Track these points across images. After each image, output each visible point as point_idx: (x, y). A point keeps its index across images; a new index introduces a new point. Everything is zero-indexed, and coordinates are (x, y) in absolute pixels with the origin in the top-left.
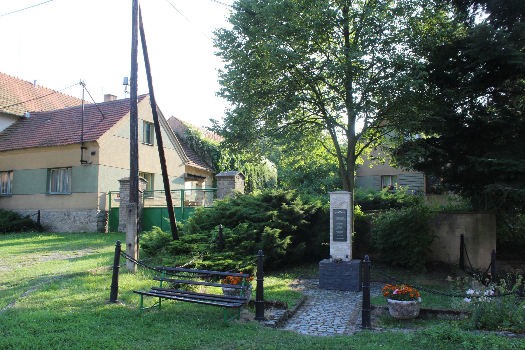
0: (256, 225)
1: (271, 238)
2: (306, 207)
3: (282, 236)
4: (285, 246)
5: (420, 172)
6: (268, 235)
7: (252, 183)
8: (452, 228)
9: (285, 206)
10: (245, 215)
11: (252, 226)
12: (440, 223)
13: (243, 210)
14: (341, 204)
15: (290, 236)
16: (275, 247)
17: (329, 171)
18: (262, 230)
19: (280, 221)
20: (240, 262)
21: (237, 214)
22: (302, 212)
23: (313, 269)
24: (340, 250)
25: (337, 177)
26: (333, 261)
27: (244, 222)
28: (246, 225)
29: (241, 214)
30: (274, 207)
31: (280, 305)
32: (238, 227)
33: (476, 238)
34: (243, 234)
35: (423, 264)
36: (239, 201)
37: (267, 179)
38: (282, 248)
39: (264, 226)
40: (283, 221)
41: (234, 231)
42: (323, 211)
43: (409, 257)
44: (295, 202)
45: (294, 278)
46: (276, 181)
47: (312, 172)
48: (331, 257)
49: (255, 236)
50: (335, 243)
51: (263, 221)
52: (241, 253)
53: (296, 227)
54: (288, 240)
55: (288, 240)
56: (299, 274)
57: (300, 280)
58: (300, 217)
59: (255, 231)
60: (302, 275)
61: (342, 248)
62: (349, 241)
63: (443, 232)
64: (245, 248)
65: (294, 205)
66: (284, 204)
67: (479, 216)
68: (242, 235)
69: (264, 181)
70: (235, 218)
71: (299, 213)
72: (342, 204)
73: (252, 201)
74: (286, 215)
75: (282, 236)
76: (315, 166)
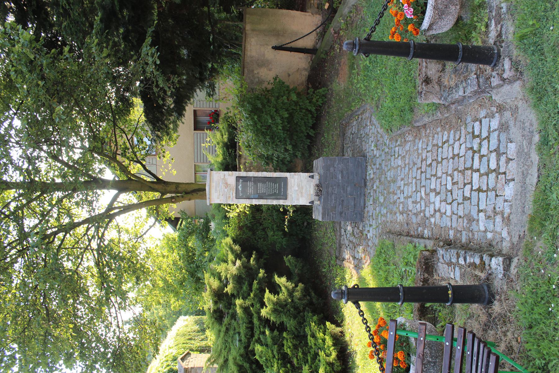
0: (258, 332)
1: (279, 307)
2: (231, 257)
3: (275, 289)
4: (290, 285)
5: (187, 108)
6: (275, 311)
7: (200, 346)
8: (264, 63)
9: (229, 289)
10: (242, 351)
11: (259, 338)
12: (257, 80)
13: (234, 353)
14: (227, 185)
15: (276, 277)
16: (292, 301)
17: (186, 246)
18: (266, 322)
19: (252, 295)
20: (322, 354)
21: (240, 363)
22: (238, 263)
23: (323, 244)
24: (300, 189)
25: (194, 237)
26: (319, 200)
27: (253, 350)
28: (258, 348)
29: (241, 355)
30: (230, 305)
31: (426, 264)
32: (262, 361)
33: (277, 33)
34: (272, 351)
35: (314, 92)
36: (221, 360)
37: (197, 328)
38: (294, 290)
39: (260, 318)
40: (251, 291)
41: (267, 367)
42: (237, 236)
43: (304, 111)
44: (223, 274)
45: (342, 268)
46: (199, 317)
47: (186, 266)
48: (312, 202)
49: (276, 333)
50: (289, 197)
51: (251, 322)
52: (305, 354)
53: (261, 271)
54: (282, 281)
55: (282, 281)
56: (332, 262)
57: (344, 259)
58: (246, 266)
59: (267, 332)
60: (334, 258)
61: (298, 186)
62: (287, 175)
63: (267, 75)
64: (295, 347)
65: (228, 276)
66: (226, 289)
67: (248, 27)
68: (275, 353)
69: (199, 332)
70: (246, 365)
71: (240, 267)
72: (226, 183)
73: (220, 341)
74: (242, 288)
75: (275, 289)
76: (179, 263)
